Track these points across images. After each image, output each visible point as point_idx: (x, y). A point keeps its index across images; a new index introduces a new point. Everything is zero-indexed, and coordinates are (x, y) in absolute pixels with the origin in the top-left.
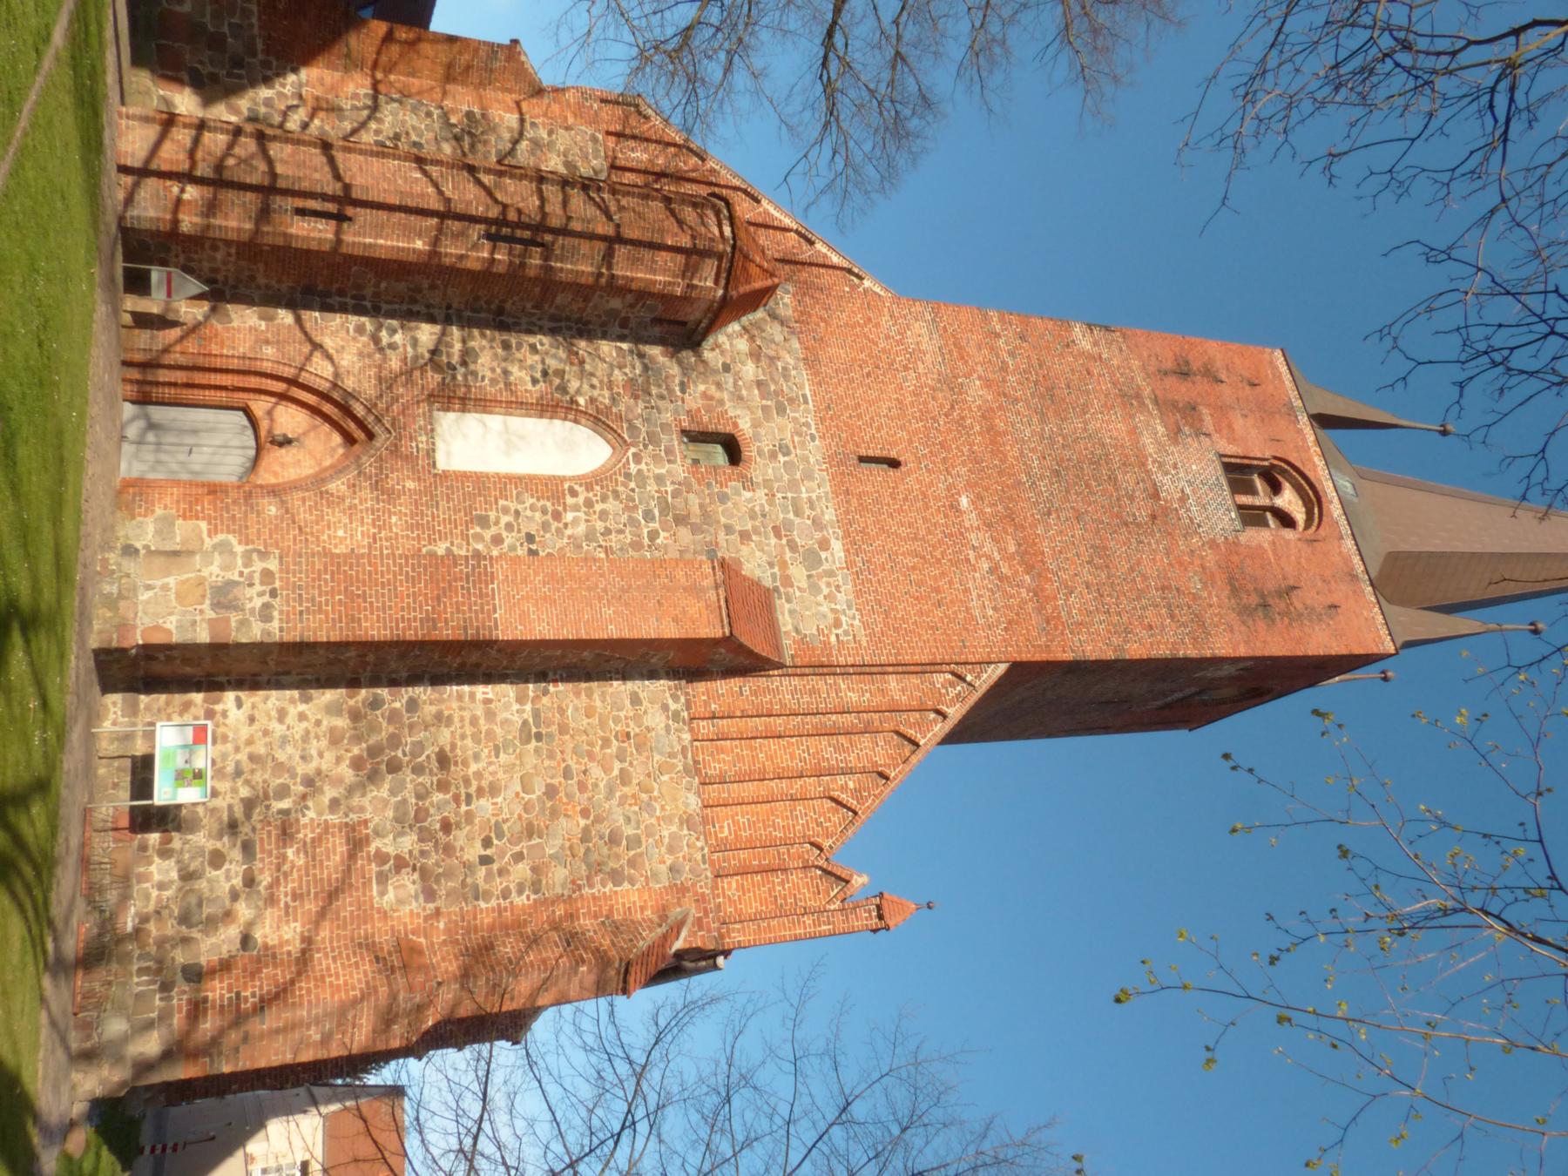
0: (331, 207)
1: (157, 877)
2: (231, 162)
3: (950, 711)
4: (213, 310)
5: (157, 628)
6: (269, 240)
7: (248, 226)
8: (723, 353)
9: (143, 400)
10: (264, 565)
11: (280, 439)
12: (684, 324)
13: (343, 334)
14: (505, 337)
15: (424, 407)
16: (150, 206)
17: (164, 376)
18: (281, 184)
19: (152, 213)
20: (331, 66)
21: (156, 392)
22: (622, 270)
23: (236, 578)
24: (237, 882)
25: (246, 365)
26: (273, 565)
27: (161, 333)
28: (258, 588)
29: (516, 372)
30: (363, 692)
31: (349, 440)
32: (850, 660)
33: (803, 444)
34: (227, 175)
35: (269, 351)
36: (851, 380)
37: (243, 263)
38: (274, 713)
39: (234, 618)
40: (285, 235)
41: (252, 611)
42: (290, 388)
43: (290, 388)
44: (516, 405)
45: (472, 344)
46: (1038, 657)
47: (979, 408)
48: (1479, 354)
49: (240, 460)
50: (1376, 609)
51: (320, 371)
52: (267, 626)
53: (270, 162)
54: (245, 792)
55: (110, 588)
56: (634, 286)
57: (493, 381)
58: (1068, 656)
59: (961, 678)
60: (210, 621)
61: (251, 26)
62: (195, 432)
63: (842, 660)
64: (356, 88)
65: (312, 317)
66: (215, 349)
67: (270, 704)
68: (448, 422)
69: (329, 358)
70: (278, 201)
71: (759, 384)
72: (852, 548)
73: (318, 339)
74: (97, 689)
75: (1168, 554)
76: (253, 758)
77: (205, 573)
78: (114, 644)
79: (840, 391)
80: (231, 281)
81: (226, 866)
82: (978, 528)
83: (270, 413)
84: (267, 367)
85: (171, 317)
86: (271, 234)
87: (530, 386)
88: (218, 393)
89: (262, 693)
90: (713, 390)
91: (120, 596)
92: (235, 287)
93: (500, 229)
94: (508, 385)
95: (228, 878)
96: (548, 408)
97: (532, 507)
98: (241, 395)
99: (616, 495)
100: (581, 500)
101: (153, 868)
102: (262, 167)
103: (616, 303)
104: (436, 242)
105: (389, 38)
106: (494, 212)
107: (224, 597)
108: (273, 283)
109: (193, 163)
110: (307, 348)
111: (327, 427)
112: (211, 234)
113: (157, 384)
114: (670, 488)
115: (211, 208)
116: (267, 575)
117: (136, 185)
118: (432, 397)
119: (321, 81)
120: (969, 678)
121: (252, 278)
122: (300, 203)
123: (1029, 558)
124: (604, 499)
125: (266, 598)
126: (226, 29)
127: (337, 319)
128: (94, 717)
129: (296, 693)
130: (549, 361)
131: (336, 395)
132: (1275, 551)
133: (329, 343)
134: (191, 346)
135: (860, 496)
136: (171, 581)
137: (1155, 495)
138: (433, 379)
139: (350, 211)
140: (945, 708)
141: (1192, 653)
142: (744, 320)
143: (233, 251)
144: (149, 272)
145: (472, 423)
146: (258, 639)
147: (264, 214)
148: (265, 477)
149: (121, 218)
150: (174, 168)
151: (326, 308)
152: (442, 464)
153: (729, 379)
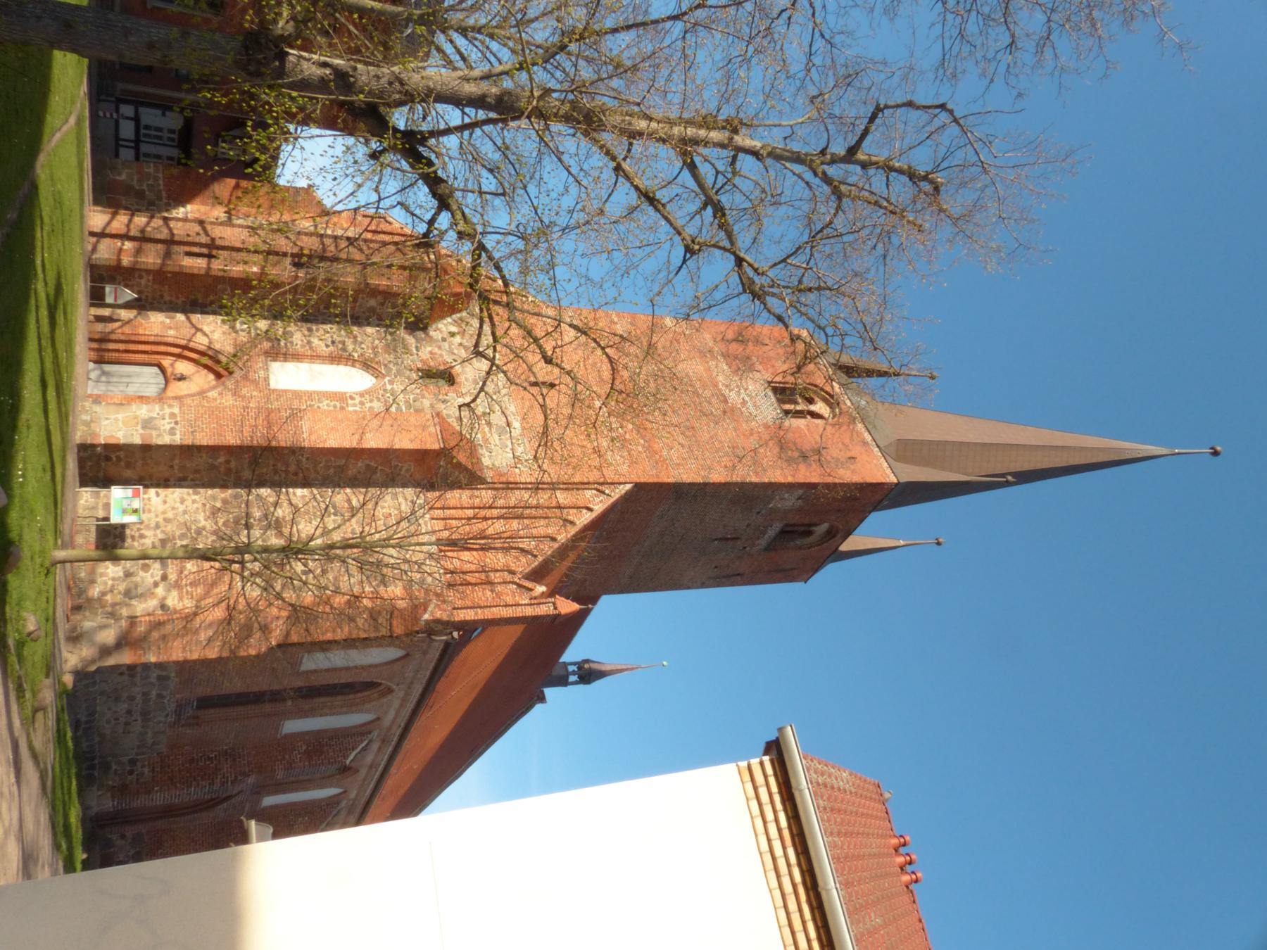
0: (205, 251)
1: (111, 575)
2: (149, 229)
3: (595, 508)
4: (139, 314)
5: (112, 436)
6: (169, 269)
7: (159, 261)
8: (441, 332)
9: (100, 361)
10: (171, 410)
11: (179, 376)
13: (213, 324)
14: (309, 325)
15: (262, 358)
16: (105, 252)
17: (111, 346)
18: (176, 238)
19: (106, 256)
20: (203, 204)
21: (107, 355)
22: (374, 281)
23: (155, 415)
24: (158, 578)
25: (159, 339)
26: (176, 410)
27: (110, 325)
28: (168, 420)
29: (315, 341)
30: (230, 491)
31: (218, 376)
32: (528, 480)
34: (147, 235)
35: (172, 332)
37: (156, 286)
38: (178, 500)
39: (154, 433)
40: (180, 266)
41: (165, 431)
42: (184, 351)
43: (184, 351)
44: (315, 357)
45: (289, 329)
46: (651, 481)
48: (590, 93)
49: (156, 390)
50: (883, 459)
51: (200, 341)
52: (173, 437)
53: (170, 229)
54: (161, 536)
55: (85, 417)
56: (381, 288)
57: (303, 346)
58: (671, 480)
59: (603, 493)
60: (141, 434)
61: (159, 185)
62: (129, 376)
63: (523, 480)
64: (219, 213)
65: (196, 318)
66: (141, 332)
67: (175, 495)
68: (275, 366)
69: (206, 335)
70: (176, 248)
73: (200, 327)
74: (78, 484)
75: (735, 430)
76: (165, 520)
77: (138, 413)
78: (89, 442)
80: (150, 300)
81: (151, 571)
83: (172, 365)
84: (170, 340)
85: (115, 317)
86: (171, 266)
87: (325, 348)
88: (143, 356)
89: (171, 490)
90: (436, 350)
91: (92, 421)
92: (152, 303)
93: (299, 261)
94: (311, 348)
95: (152, 576)
96: (334, 359)
97: (328, 405)
98: (156, 356)
99: (379, 399)
100: (357, 401)
101: (109, 571)
102: (166, 231)
103: (372, 303)
104: (263, 268)
105: (237, 186)
106: (296, 250)
107: (147, 424)
108: (174, 299)
109: (129, 230)
110: (193, 331)
111: (205, 371)
112: (137, 267)
113: (109, 350)
114: (411, 397)
115: (138, 252)
116: (173, 415)
117: (98, 242)
118: (267, 353)
119: (199, 210)
120: (607, 491)
121: (162, 296)
122: (187, 249)
124: (371, 401)
125: (173, 425)
126: (145, 187)
127: (211, 318)
128: (76, 497)
129: (191, 491)
130: (335, 337)
131: (210, 353)
132: (808, 430)
133: (206, 328)
134: (127, 329)
136: (120, 416)
137: (725, 401)
138: (266, 345)
139: (214, 252)
140: (591, 506)
141: (755, 479)
142: (454, 316)
143: (151, 278)
144: (103, 288)
145: (290, 367)
146: (168, 443)
147: (168, 255)
148: (170, 393)
149: (90, 259)
150: (119, 232)
151: (203, 313)
152: (273, 385)
153: (446, 345)
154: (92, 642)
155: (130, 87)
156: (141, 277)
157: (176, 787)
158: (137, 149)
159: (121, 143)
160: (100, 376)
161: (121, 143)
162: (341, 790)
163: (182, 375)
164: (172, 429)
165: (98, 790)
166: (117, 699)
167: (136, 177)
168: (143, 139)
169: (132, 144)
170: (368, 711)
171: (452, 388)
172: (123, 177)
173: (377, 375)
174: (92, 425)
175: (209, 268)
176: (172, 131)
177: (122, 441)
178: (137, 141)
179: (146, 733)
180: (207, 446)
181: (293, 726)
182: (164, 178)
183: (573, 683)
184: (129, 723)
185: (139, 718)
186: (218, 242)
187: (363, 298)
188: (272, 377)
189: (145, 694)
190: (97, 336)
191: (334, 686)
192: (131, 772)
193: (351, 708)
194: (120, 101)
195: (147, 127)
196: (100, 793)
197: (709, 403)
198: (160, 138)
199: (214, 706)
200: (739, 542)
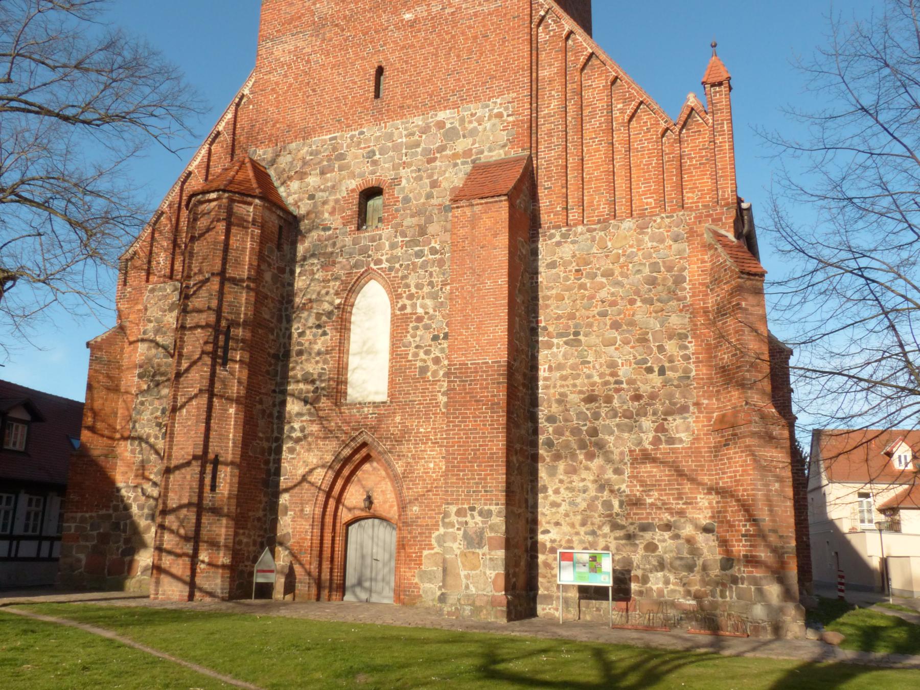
0: (209, 468)
1: (661, 585)
2: (182, 531)
3: (567, 28)
6: (233, 508)
7: (224, 521)
8: (301, 200)
9: (342, 589)
10: (453, 514)
11: (367, 503)
14: (294, 353)
17: (326, 575)
18: (195, 500)
22: (244, 272)
23: (461, 532)
25: (318, 524)
26: (453, 509)
31: (367, 458)
32: (527, 106)
34: (191, 534)
35: (308, 509)
40: (229, 498)
44: (342, 347)
45: (299, 376)
49: (382, 529)
51: (320, 477)
54: (606, 529)
55: (467, 610)
57: (325, 362)
59: (543, 18)
61: (91, 517)
63: (527, 112)
64: (127, 451)
66: (307, 544)
68: (354, 393)
69: (311, 471)
70: (207, 502)
73: (299, 478)
76: (583, 524)
77: (458, 552)
78: (505, 609)
80: (262, 533)
81: (656, 542)
84: (318, 511)
86: (229, 507)
87: (328, 337)
90: (328, 207)
95: (664, 541)
96: (343, 326)
98: (338, 528)
99: (404, 277)
100: (408, 302)
101: (654, 587)
102: (184, 511)
103: (268, 276)
104: (229, 399)
105: (92, 429)
107: (474, 540)
108: (262, 506)
113: (331, 580)
115: (213, 544)
116: (459, 513)
117: (201, 590)
120: (542, 13)
121: (259, 519)
122: (207, 488)
124: (407, 286)
125: (476, 513)
126: (95, 533)
127: (285, 465)
128: (552, 622)
129: (540, 496)
131: (337, 467)
133: (301, 471)
136: (463, 573)
138: (324, 403)
140: (565, 33)
143: (241, 531)
144: (257, 584)
147: (216, 511)
152: (383, 397)
154: (781, 610)
156: (240, 543)
158: (20, 538)
159: (13, 555)
160: (365, 589)
161: (13, 555)
163: (365, 500)
164: (481, 513)
167: (82, 543)
168: (8, 532)
169: (15, 543)
171: (386, 190)
172: (82, 556)
173: (368, 275)
174: (478, 603)
175: (232, 463)
177: (501, 571)
178: (40, 538)
180: (507, 474)
182: (92, 511)
186: (199, 452)
188: (372, 398)
190: (314, 591)
198: (36, 515)
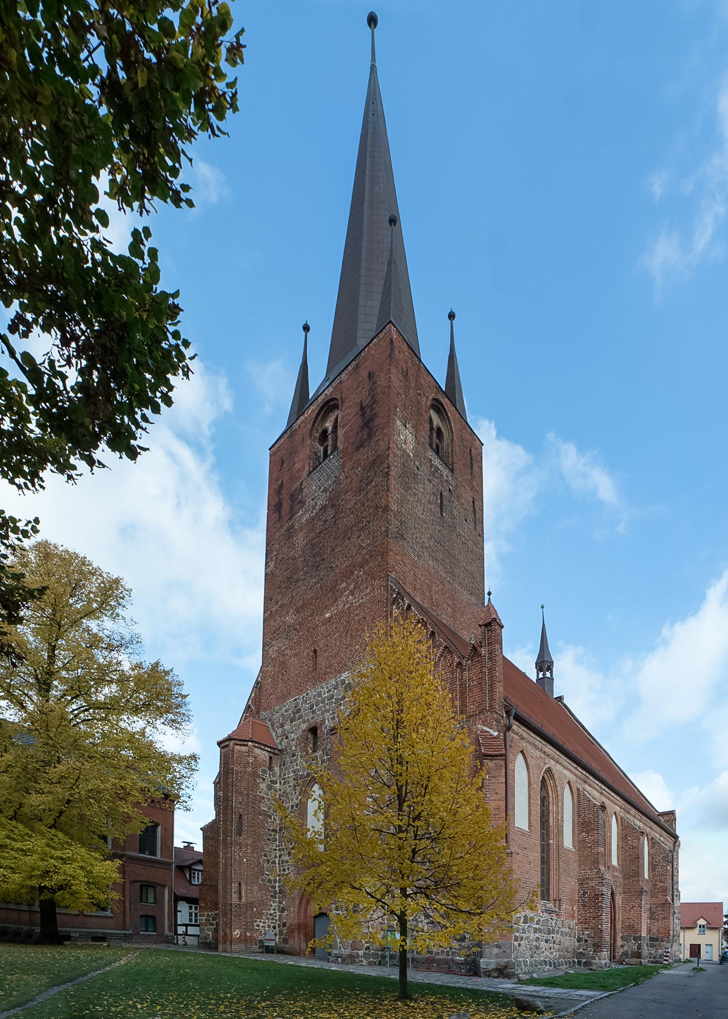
12: (270, 758)
33: (310, 699)
36: (288, 679)
47: (295, 615)
71: (291, 722)
72: (343, 668)
79: (292, 684)
82: (337, 605)
123: (347, 574)
135: (326, 668)
155: (166, 927)
157: (601, 915)
162: (614, 817)
165: (595, 959)
166: (537, 948)
170: (563, 789)
176: (191, 908)
179: (562, 931)
181: (568, 841)
183: (552, 675)
184: (555, 941)
185: (551, 935)
187: (261, 792)
189: (535, 932)
191: (542, 812)
192: (586, 941)
193: (559, 801)
194: (176, 933)
195: (191, 920)
196: (597, 958)
197: (326, 521)
199: (548, 890)
200: (444, 494)
